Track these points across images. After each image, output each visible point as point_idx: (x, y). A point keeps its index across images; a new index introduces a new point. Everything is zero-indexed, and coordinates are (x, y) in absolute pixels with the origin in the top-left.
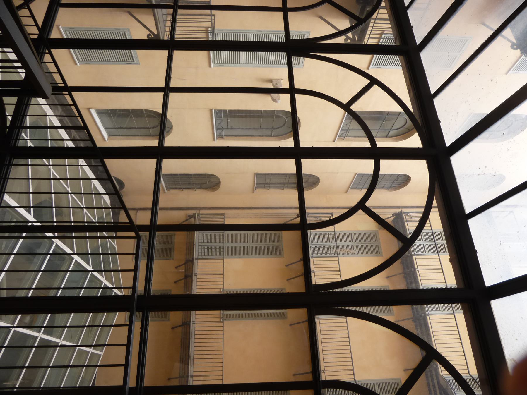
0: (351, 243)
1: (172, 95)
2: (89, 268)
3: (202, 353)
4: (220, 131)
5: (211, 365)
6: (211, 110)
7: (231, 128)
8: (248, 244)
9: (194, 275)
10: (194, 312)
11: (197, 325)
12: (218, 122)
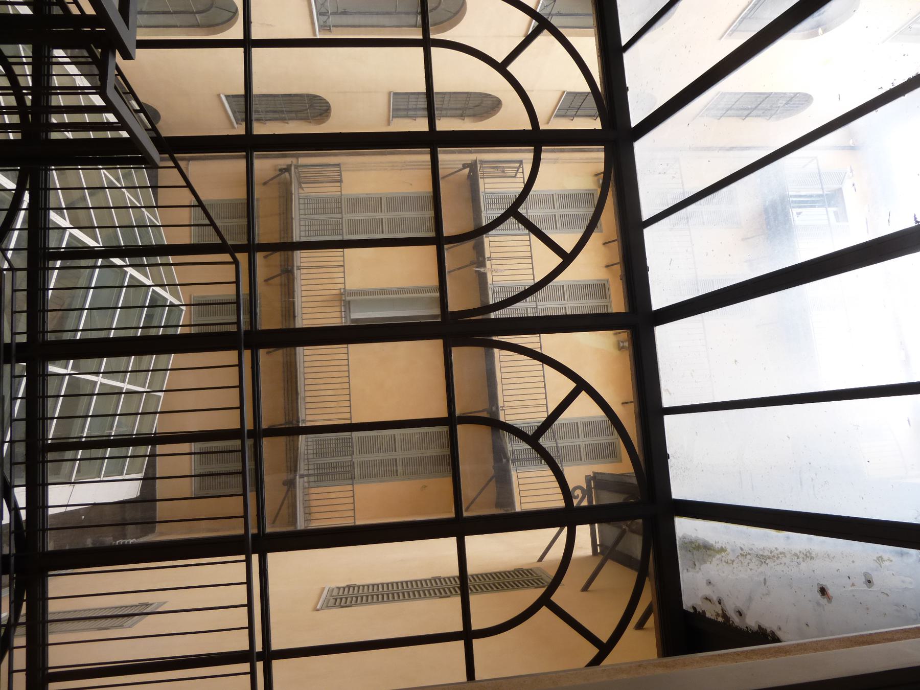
0: (553, 210)
1: (256, 52)
2: (148, 282)
3: (317, 387)
4: (324, 18)
5: (333, 404)
7: (345, 13)
8: (383, 214)
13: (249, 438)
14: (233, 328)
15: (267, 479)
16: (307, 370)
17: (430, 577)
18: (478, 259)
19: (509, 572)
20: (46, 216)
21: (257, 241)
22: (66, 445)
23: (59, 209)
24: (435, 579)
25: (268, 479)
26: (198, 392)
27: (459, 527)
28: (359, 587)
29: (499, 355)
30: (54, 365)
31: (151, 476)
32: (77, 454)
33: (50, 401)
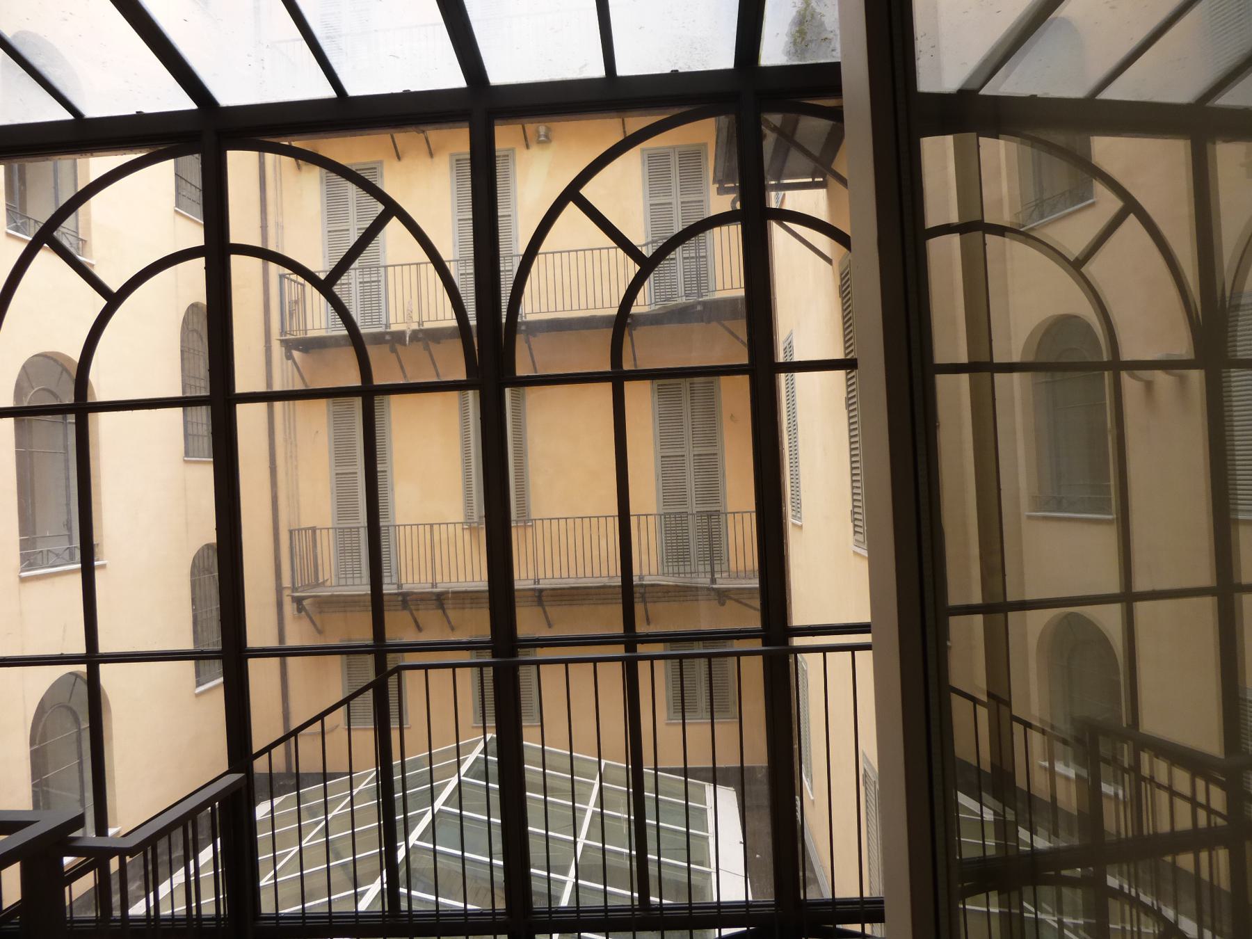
2: (454, 782)
6: (23, 580)
9: (435, 590)
10: (384, 587)
11: (541, 575)
12: (53, 559)
13: (635, 651)
14: (489, 672)
15: (705, 625)
16: (573, 574)
17: (846, 412)
18: (386, 342)
19: (843, 304)
20: (367, 915)
21: (371, 642)
22: (641, 878)
23: (357, 897)
24: (848, 406)
25: (705, 624)
26: (574, 719)
27: (764, 369)
28: (854, 507)
29: (533, 308)
30: (559, 898)
31: (711, 775)
32: (653, 860)
33: (612, 902)
